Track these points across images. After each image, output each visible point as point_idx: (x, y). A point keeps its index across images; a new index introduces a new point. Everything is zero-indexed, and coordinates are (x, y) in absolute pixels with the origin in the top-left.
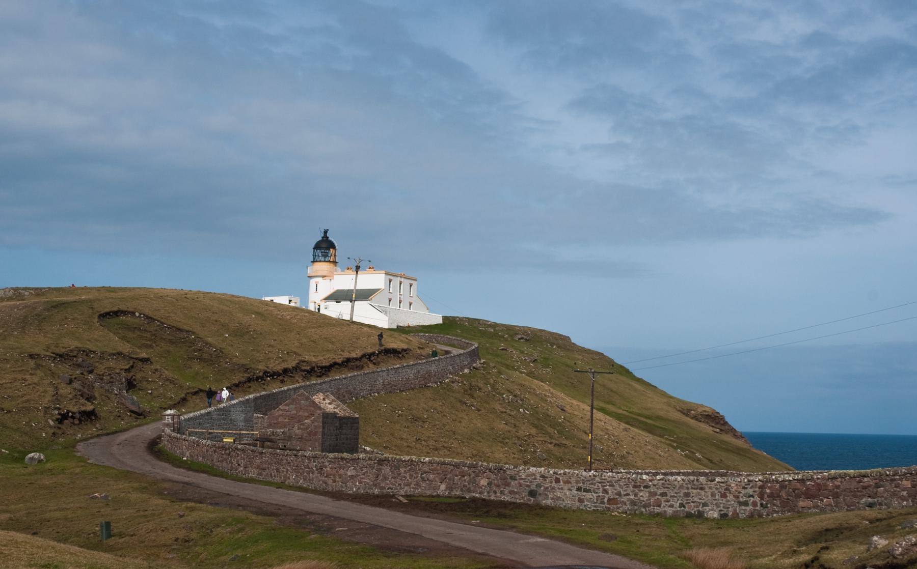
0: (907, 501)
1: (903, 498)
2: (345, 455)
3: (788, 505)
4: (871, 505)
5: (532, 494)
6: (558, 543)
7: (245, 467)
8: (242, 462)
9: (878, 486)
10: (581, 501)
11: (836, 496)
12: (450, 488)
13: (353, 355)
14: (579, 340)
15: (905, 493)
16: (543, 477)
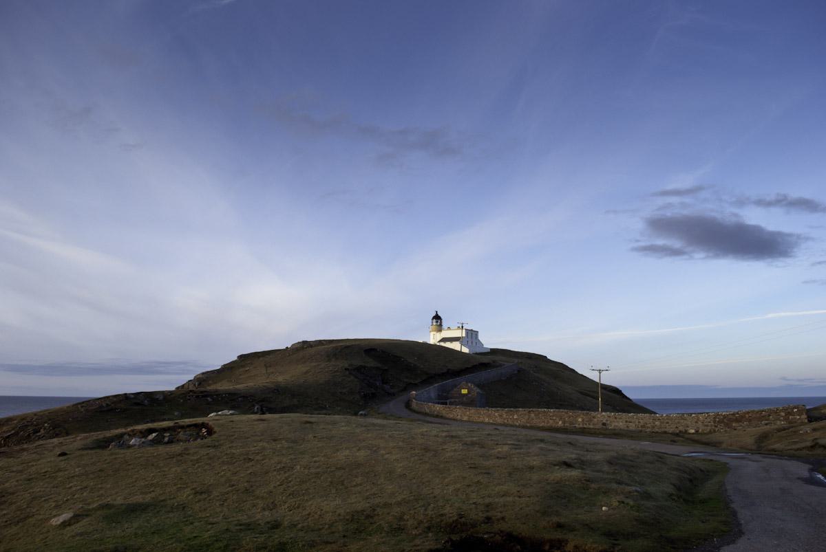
0: (564, 419)
1: (781, 420)
2: (512, 409)
3: (728, 425)
4: (766, 424)
5: (604, 424)
6: (606, 441)
7: (461, 416)
8: (459, 414)
9: (769, 416)
10: (627, 427)
11: (750, 421)
12: (564, 422)
13: (469, 366)
14: (552, 357)
15: (782, 418)
16: (609, 417)
